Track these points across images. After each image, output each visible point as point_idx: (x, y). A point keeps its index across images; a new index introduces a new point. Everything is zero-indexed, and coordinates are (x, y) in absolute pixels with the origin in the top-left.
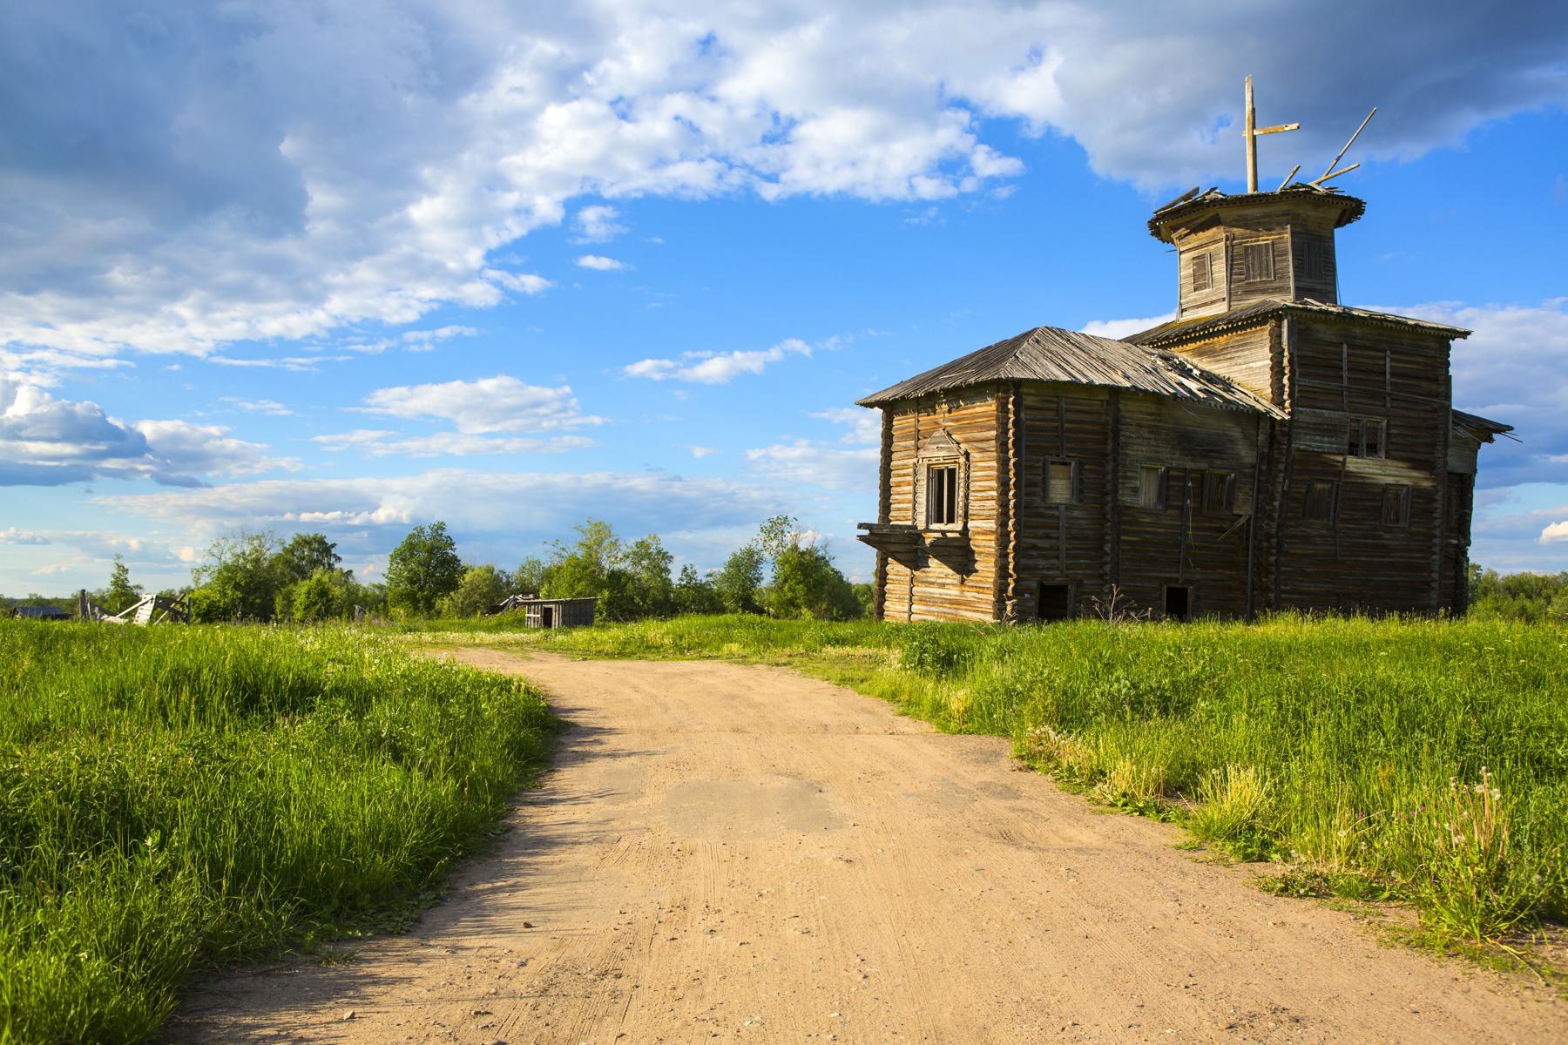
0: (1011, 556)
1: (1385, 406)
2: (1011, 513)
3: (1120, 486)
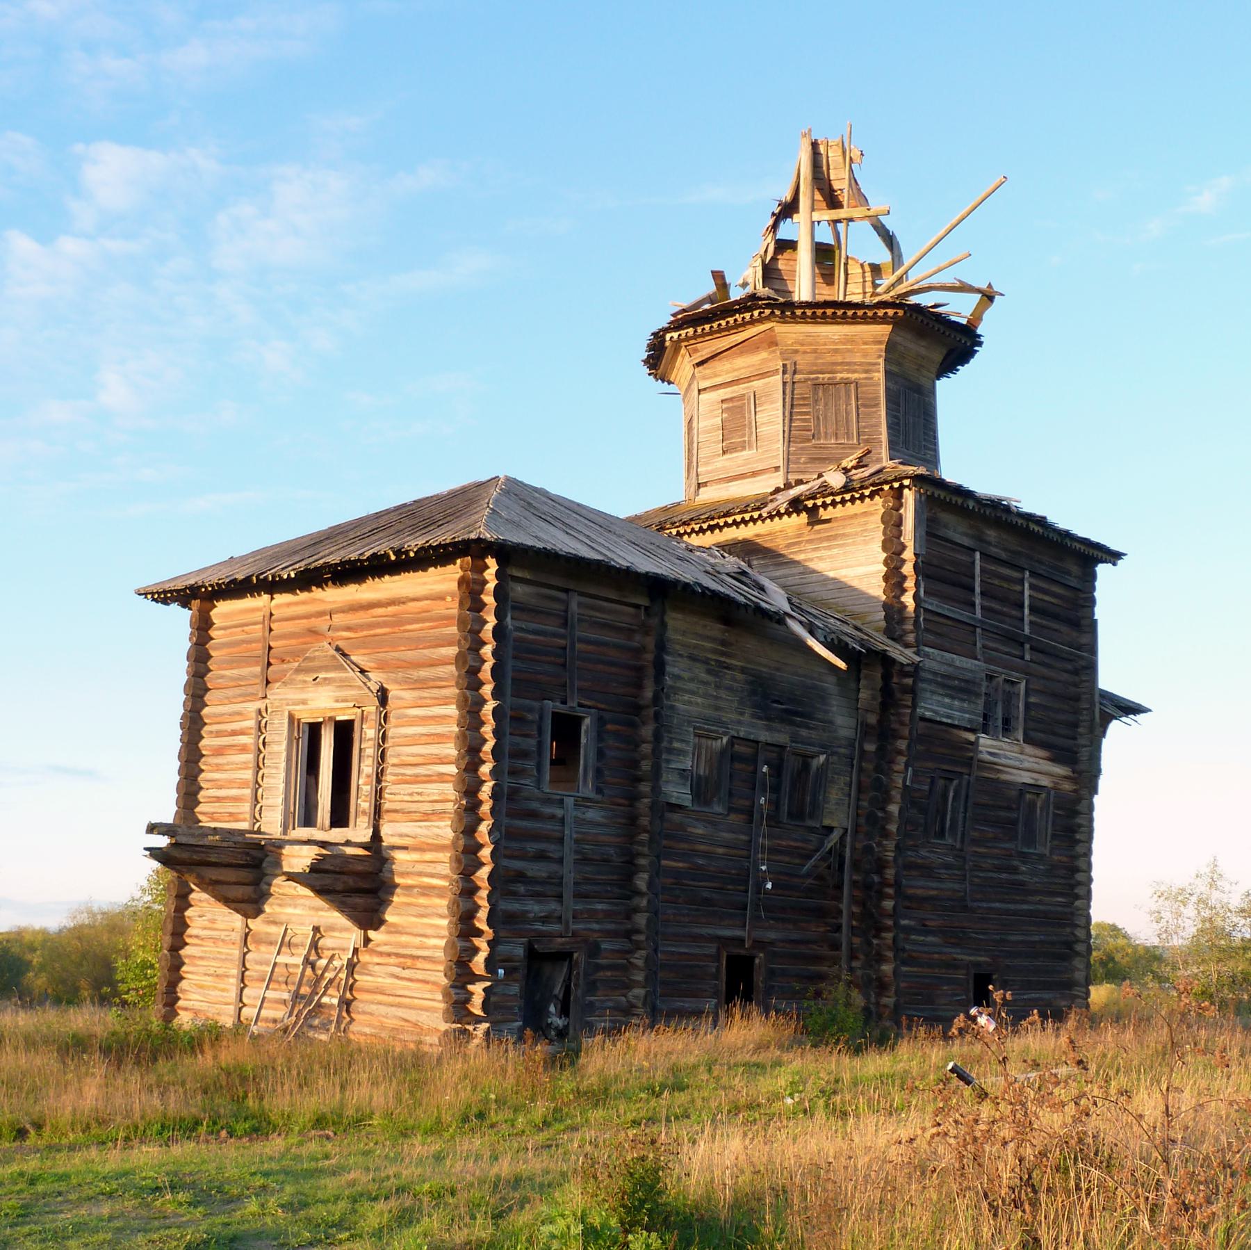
0: (484, 893)
1: (1022, 658)
2: (486, 808)
3: (664, 765)
